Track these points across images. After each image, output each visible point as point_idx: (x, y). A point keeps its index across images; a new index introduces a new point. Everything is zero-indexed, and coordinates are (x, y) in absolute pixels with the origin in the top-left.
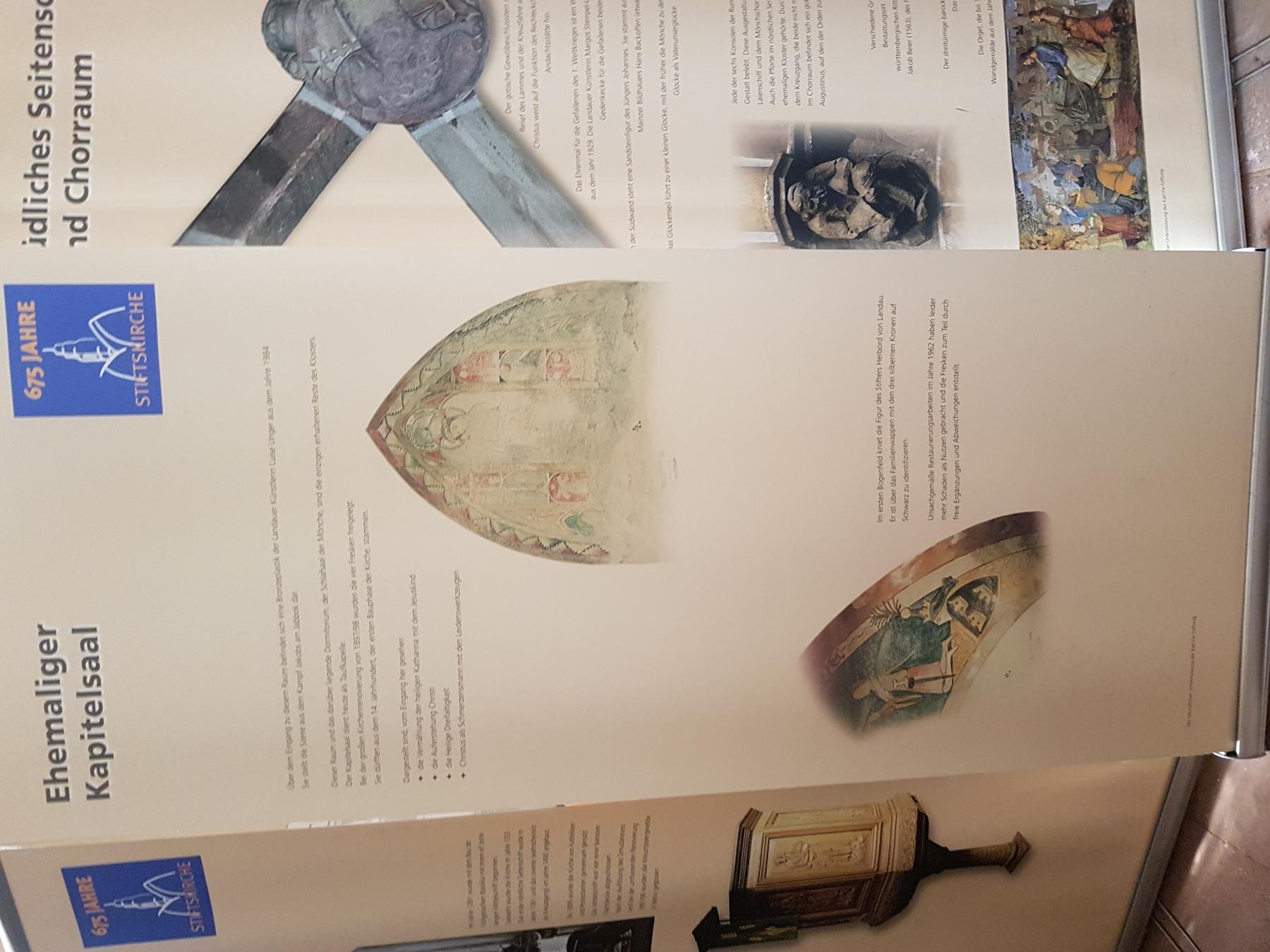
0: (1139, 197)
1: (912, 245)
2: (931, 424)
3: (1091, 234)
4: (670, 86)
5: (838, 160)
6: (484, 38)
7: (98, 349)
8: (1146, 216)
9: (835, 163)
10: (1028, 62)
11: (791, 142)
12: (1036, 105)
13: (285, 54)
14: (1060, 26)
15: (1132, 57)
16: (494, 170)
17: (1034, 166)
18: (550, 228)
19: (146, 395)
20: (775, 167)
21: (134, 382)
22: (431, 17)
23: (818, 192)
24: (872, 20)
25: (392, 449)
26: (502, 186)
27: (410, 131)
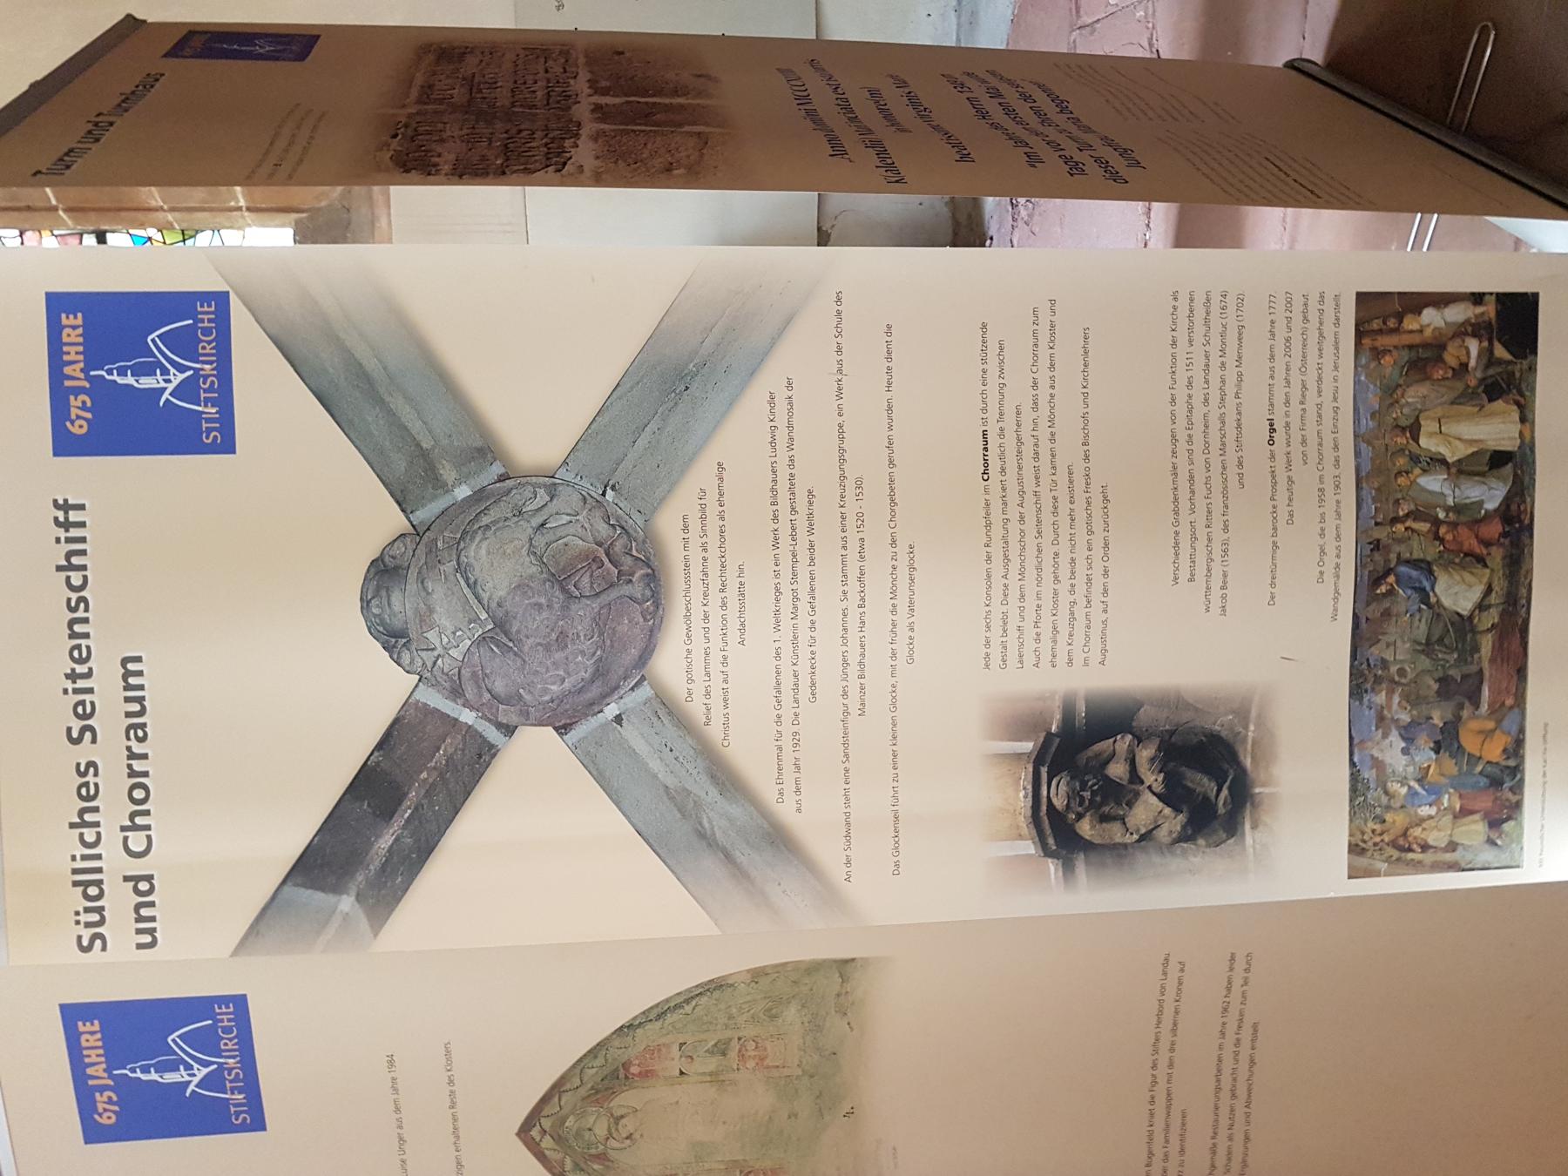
0: (1512, 763)
1: (1208, 846)
2: (1218, 1089)
3: (1443, 816)
4: (903, 652)
5: (1119, 737)
6: (657, 605)
7: (182, 1067)
8: (1518, 788)
9: (1115, 742)
10: (1383, 589)
11: (1058, 716)
12: (1388, 645)
13: (393, 640)
14: (1431, 536)
15: (1523, 572)
16: (670, 781)
17: (1377, 729)
18: (743, 855)
19: (214, 375)
20: (1036, 753)
21: (228, 1099)
22: (586, 580)
23: (1090, 783)
24: (1177, 544)
25: (547, 1152)
26: (680, 800)
27: (561, 734)
